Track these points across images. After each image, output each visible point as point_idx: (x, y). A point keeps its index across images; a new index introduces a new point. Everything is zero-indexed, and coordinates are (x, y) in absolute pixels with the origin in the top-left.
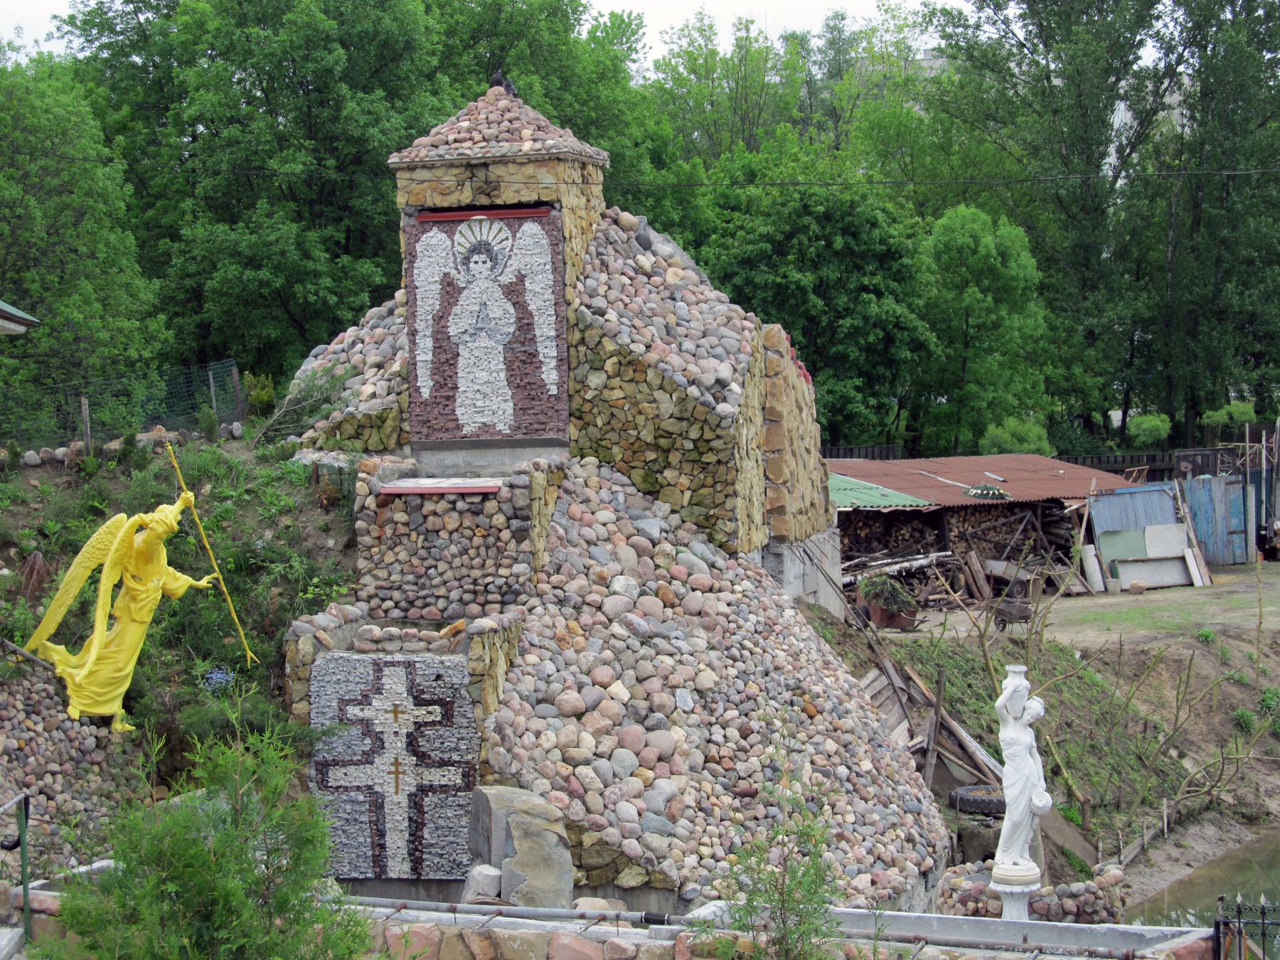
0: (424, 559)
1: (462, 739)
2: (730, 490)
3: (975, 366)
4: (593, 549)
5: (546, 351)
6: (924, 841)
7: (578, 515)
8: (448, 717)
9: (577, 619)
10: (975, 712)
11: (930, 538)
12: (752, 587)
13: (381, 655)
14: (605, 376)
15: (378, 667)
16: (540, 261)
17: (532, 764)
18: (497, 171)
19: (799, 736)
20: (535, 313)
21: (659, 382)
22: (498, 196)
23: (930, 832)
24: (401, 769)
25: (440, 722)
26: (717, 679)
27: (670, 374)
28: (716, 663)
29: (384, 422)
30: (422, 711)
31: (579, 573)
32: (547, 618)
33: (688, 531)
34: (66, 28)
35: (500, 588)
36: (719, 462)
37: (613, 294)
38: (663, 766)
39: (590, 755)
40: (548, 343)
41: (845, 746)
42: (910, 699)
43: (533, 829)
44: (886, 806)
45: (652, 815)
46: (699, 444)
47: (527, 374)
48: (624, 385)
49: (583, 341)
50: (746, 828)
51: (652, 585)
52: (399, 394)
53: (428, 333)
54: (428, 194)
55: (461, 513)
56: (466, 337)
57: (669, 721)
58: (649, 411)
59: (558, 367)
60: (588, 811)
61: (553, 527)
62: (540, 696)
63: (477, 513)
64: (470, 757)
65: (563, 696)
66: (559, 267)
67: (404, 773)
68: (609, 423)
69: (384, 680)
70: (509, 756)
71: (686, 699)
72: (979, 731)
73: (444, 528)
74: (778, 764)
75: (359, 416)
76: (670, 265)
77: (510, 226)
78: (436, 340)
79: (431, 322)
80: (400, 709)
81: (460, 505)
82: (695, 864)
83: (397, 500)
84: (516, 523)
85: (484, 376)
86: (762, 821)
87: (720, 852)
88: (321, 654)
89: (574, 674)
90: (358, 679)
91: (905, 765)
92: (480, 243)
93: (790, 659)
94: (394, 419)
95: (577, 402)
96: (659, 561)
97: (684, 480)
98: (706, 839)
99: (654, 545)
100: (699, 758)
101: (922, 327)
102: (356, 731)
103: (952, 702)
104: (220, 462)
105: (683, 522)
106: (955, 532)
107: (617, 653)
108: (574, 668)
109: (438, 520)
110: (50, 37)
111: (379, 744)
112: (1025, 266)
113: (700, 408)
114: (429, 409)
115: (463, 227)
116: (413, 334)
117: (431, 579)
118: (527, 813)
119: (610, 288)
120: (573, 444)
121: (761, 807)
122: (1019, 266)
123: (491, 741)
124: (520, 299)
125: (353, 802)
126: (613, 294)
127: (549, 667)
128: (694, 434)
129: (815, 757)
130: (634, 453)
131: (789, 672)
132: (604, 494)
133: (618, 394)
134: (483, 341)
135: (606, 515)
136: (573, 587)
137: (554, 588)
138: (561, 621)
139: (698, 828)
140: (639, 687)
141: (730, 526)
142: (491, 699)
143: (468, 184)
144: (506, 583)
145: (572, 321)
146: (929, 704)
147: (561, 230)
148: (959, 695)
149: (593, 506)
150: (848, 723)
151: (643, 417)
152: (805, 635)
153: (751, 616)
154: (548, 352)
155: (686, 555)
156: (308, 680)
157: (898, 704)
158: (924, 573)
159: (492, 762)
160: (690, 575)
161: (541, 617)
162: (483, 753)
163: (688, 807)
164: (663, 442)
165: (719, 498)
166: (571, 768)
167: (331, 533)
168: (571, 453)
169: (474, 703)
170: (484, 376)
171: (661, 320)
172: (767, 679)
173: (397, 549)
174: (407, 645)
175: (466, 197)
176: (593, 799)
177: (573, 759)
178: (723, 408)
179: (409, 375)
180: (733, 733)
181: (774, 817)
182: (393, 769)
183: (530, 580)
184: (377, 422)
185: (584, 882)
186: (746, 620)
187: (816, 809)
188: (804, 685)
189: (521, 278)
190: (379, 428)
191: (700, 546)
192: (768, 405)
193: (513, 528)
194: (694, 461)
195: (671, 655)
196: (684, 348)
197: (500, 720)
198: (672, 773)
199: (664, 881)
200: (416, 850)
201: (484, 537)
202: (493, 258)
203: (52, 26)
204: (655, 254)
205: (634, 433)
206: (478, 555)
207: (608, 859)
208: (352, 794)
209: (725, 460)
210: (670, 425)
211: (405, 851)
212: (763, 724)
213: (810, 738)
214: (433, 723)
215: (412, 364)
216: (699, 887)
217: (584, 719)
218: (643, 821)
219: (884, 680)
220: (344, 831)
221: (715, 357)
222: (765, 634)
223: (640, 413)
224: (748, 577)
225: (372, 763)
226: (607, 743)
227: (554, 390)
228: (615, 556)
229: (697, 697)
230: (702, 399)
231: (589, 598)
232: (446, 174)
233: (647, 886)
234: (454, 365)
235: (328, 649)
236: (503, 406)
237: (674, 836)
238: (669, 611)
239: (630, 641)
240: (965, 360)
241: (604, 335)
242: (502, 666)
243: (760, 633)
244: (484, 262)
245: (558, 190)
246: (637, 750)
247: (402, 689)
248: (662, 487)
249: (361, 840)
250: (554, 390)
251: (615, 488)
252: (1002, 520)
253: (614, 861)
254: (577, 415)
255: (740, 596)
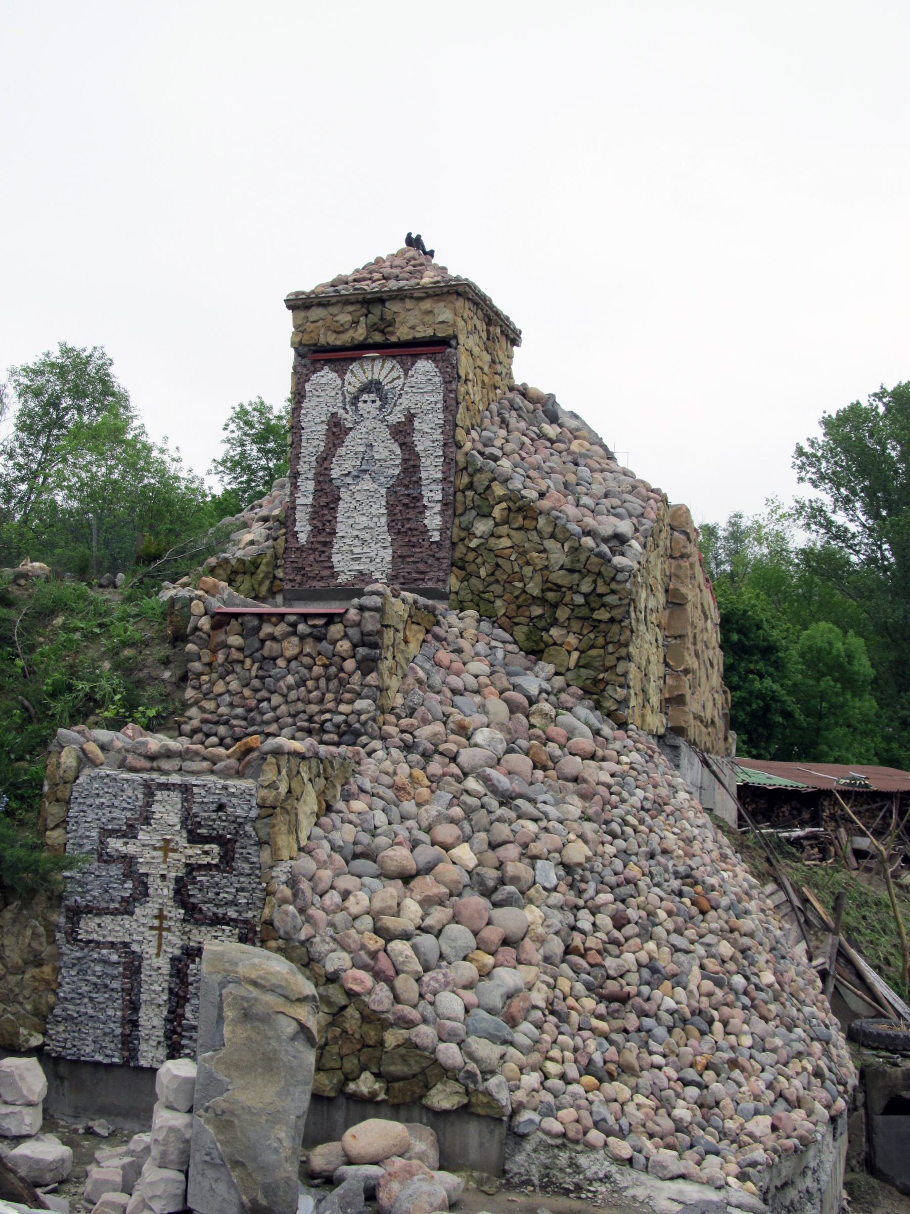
0: (256, 691)
1: (242, 890)
2: (623, 652)
3: (826, 733)
4: (457, 699)
5: (431, 494)
6: (833, 1077)
7: (446, 662)
8: (227, 859)
9: (424, 769)
10: (871, 942)
11: (806, 816)
12: (642, 761)
13: (155, 775)
14: (492, 523)
15: (149, 789)
16: (432, 399)
17: (330, 931)
18: (393, 307)
19: (686, 932)
20: (422, 454)
21: (550, 529)
22: (392, 333)
23: (841, 1066)
24: (166, 924)
25: (216, 866)
26: (590, 854)
27: (564, 521)
28: (590, 835)
29: (257, 568)
30: (196, 850)
31: (435, 720)
32: (388, 763)
33: (572, 695)
34: (221, 468)
35: (338, 726)
36: (612, 620)
37: (509, 447)
38: (508, 953)
39: (411, 927)
40: (433, 486)
41: (743, 952)
42: (807, 921)
43: (259, 1009)
44: (790, 1030)
45: (483, 1014)
46: (591, 598)
47: (409, 519)
48: (513, 533)
49: (471, 486)
50: (611, 1042)
51: (523, 743)
52: (275, 539)
53: (310, 476)
54: (322, 331)
55: (302, 638)
56: (349, 480)
57: (523, 898)
58: (537, 561)
59: (442, 513)
60: (397, 999)
61: (412, 668)
62: (359, 849)
63: (319, 639)
64: (250, 915)
65: (389, 853)
66: (451, 405)
67: (169, 929)
68: (493, 574)
69: (154, 808)
70: (300, 919)
71: (548, 873)
72: (877, 961)
73: (282, 655)
74: (661, 964)
75: (234, 562)
76: (576, 438)
77: (402, 364)
78: (318, 482)
79: (314, 464)
80: (172, 845)
81: (301, 628)
82: (537, 1085)
83: (233, 622)
84: (362, 651)
85: (364, 521)
86: (634, 1035)
87: (572, 1071)
88: (87, 771)
89: (409, 830)
90: (124, 805)
91: (812, 982)
92: (371, 382)
93: (681, 844)
94: (268, 564)
95: (461, 549)
96: (535, 720)
97: (572, 640)
98: (555, 1053)
99: (531, 703)
100: (556, 946)
101: (789, 699)
102: (115, 870)
103: (849, 930)
104: (83, 597)
105: (569, 685)
106: (826, 813)
107: (469, 812)
108: (411, 823)
109: (275, 646)
110: (209, 473)
111: (142, 892)
112: (864, 666)
113: (594, 559)
114: (304, 555)
115: (355, 366)
116: (296, 475)
117: (263, 714)
118: (254, 983)
119: (507, 441)
120: (452, 596)
121: (633, 1017)
122: (861, 665)
123: (279, 895)
124: (408, 439)
125: (105, 962)
126: (509, 447)
127: (380, 818)
128: (586, 588)
129: (706, 961)
130: (519, 607)
131: (679, 857)
132: (481, 647)
133: (505, 542)
134: (367, 484)
135: (480, 667)
136: (424, 733)
137: (403, 732)
138: (404, 769)
139: (545, 1036)
140: (490, 853)
141: (621, 693)
142: (284, 841)
143: (362, 319)
144: (346, 722)
145: (462, 464)
146: (826, 928)
147: (455, 367)
148: (855, 924)
149: (465, 656)
150: (747, 924)
151: (531, 568)
152: (700, 822)
153: (638, 791)
154: (432, 494)
155: (566, 718)
156: (68, 802)
157: (796, 924)
158: (801, 844)
159: (276, 923)
160: (569, 739)
161: (380, 761)
162: (267, 911)
163: (535, 1007)
164: (550, 595)
165: (610, 660)
166: (382, 942)
167: (172, 666)
168: (450, 605)
169: (261, 843)
170: (364, 521)
171: (560, 476)
172: (652, 862)
173: (228, 679)
174: (188, 765)
175: (360, 334)
176: (406, 985)
177: (387, 930)
178: (618, 560)
179: (286, 521)
180: (604, 920)
181: (649, 1031)
182: (156, 923)
183: (374, 720)
184: (248, 568)
185: (382, 1096)
186: (632, 794)
187: (704, 1027)
188: (695, 873)
189: (410, 417)
190: (252, 574)
191: (583, 710)
192: (671, 586)
193: (359, 657)
194: (584, 619)
195: (536, 820)
196: (581, 502)
197: (296, 871)
198: (519, 962)
199: (488, 1105)
200: (174, 1032)
201: (326, 666)
202: (384, 399)
203: (211, 466)
204: (561, 426)
205: (520, 585)
206: (317, 688)
207: (416, 1069)
208: (104, 951)
209: (619, 617)
210: (560, 577)
211: (161, 1033)
212: (643, 914)
213: (701, 936)
214: (208, 867)
215: (292, 508)
216: (536, 1117)
217: (413, 884)
218: (469, 1020)
219: (781, 897)
220: (91, 999)
221: (615, 515)
222: (653, 812)
223: (528, 563)
224: (638, 750)
225: (131, 913)
226: (438, 915)
227: (436, 536)
228: (483, 709)
229: (562, 872)
230: (597, 550)
231: (442, 748)
232: (342, 312)
233: (465, 1111)
234: (334, 509)
235: (95, 764)
236: (382, 553)
237: (511, 1044)
238: (539, 774)
239: (485, 799)
240: (818, 730)
241: (494, 479)
242: (309, 803)
243: (647, 811)
244: (374, 402)
245: (454, 325)
246: (475, 928)
247: (175, 819)
248: (547, 646)
249: (110, 1012)
250: (436, 536)
251: (494, 643)
252: (865, 807)
253: (423, 1071)
254: (460, 565)
255: (626, 767)
